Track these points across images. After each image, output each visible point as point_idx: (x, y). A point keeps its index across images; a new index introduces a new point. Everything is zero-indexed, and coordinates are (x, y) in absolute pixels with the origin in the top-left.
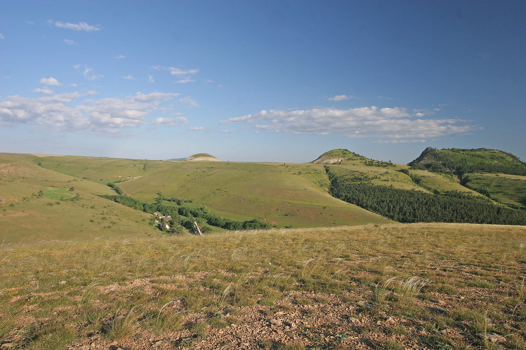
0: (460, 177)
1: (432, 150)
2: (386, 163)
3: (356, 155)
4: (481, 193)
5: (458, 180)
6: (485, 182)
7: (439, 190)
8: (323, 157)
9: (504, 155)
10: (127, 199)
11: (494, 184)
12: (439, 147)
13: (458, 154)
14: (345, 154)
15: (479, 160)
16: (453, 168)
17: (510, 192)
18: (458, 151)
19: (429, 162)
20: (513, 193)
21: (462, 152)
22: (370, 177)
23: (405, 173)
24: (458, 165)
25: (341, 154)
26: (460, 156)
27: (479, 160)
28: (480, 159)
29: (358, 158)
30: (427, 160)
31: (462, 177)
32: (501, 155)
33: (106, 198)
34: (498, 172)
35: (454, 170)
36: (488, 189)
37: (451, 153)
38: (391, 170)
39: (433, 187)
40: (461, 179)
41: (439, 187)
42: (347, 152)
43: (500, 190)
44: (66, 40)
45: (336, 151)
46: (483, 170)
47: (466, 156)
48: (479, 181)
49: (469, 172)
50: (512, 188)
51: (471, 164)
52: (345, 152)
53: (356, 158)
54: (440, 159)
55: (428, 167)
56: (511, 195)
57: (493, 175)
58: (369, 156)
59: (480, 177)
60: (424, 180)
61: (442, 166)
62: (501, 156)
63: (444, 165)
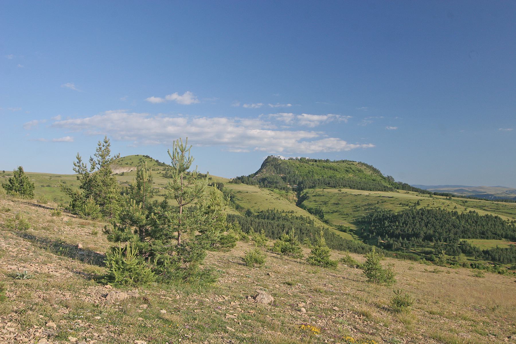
0: (298, 195)
1: (275, 159)
3: (159, 164)
5: (295, 198)
6: (323, 199)
7: (252, 210)
9: (363, 168)
11: (333, 201)
15: (330, 173)
17: (345, 211)
19: (268, 175)
20: (350, 211)
21: (312, 163)
24: (301, 179)
26: (307, 168)
27: (330, 173)
28: (332, 171)
29: (162, 168)
30: (266, 174)
32: (359, 168)
34: (345, 186)
35: (295, 186)
36: (324, 209)
39: (246, 206)
40: (299, 197)
42: (148, 159)
43: (335, 209)
44: (270, 105)
45: (130, 158)
46: (328, 185)
47: (316, 167)
48: (317, 198)
49: (310, 188)
50: (350, 206)
51: (316, 177)
54: (281, 171)
56: (347, 215)
57: (335, 191)
62: (349, 166)
63: (284, 179)
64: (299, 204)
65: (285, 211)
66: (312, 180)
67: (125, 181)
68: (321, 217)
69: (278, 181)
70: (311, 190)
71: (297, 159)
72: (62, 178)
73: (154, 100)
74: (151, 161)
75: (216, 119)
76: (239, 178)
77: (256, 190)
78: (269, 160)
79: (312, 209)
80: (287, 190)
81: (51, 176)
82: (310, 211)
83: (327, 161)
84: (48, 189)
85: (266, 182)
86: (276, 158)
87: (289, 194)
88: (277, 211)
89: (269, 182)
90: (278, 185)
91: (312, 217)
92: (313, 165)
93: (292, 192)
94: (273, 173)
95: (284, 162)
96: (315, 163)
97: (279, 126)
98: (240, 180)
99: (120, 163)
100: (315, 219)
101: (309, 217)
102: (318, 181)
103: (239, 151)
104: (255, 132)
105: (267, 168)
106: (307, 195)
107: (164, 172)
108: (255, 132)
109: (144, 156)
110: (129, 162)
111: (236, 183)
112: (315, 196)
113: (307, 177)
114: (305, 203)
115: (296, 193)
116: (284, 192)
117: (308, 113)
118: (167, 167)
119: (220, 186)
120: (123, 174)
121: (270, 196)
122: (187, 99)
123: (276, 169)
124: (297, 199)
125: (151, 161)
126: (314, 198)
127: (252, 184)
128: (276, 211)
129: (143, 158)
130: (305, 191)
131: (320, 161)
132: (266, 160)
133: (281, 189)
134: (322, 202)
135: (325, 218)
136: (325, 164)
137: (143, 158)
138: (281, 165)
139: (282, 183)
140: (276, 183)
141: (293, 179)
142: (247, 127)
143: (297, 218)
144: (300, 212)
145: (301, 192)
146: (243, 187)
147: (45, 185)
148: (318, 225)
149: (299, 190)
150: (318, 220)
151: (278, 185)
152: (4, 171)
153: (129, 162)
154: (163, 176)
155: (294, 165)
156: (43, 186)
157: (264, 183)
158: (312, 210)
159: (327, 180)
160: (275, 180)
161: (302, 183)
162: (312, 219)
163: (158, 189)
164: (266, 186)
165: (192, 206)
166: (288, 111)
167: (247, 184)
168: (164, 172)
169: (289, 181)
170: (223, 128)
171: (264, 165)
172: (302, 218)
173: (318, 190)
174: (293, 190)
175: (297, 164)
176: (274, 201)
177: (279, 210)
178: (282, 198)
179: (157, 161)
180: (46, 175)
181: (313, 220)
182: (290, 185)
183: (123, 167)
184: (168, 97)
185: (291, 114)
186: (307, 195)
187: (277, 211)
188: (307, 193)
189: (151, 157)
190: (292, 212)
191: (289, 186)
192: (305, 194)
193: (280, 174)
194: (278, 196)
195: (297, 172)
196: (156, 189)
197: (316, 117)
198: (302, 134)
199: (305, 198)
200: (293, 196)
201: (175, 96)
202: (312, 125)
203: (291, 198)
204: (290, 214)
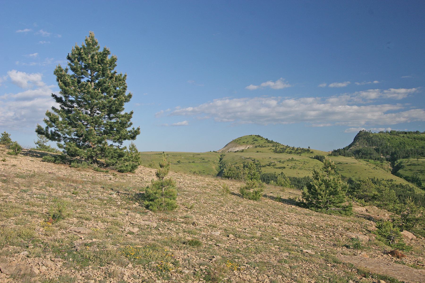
0: (392, 165)
1: (366, 133)
2: (303, 149)
3: (269, 142)
4: (409, 181)
5: (390, 167)
6: (419, 168)
7: (353, 179)
8: (229, 146)
10: (37, 156)
12: (375, 130)
13: (396, 137)
14: (256, 140)
16: (387, 153)
18: (398, 133)
19: (361, 147)
21: (402, 135)
22: (262, 164)
23: (320, 160)
24: (394, 150)
25: (251, 140)
26: (398, 139)
29: (271, 145)
30: (359, 146)
31: (394, 164)
33: (33, 156)
37: (388, 136)
38: (304, 157)
39: (348, 175)
40: (393, 167)
41: (355, 174)
42: (259, 139)
45: (246, 138)
47: (407, 139)
48: (412, 167)
49: (404, 158)
51: (408, 148)
52: (256, 139)
53: (269, 144)
54: (373, 143)
55: (358, 154)
58: (284, 142)
59: (416, 162)
60: (340, 167)
61: (375, 152)
63: (377, 150)
64: (395, 172)
65: (385, 180)
66: (404, 151)
67: (248, 157)
68: (419, 185)
69: (372, 152)
70: (405, 160)
71: (387, 132)
72: (202, 156)
73: (252, 87)
74: (262, 139)
75: (302, 100)
76: (335, 151)
77: (354, 162)
78: (361, 134)
79: (408, 177)
80: (382, 160)
81: (194, 155)
82: (406, 178)
83: (417, 132)
84: (193, 164)
85: (360, 153)
86: (367, 132)
87: (384, 164)
88: (377, 179)
89: (363, 154)
90: (372, 156)
91: (411, 185)
92: (403, 137)
93: (386, 162)
94: (366, 146)
95: (376, 136)
96: (405, 135)
97: (366, 102)
98: (336, 153)
99: (238, 142)
100: (414, 186)
101: (408, 185)
102: (411, 152)
103: (322, 125)
104: (340, 108)
105: (360, 141)
106: (402, 164)
107: (274, 148)
108: (340, 108)
109: (256, 136)
110: (246, 141)
111: (335, 155)
112: (410, 165)
113: (399, 148)
114: (400, 171)
115: (390, 163)
116: (379, 162)
117: (394, 88)
118: (275, 144)
119: (319, 158)
120: (243, 151)
121: (367, 167)
122: (279, 85)
123: (368, 142)
124: (391, 168)
125: (262, 139)
126: (409, 168)
127: (348, 155)
128: (376, 180)
129: (256, 138)
130: (399, 161)
131: (409, 133)
132: (358, 134)
133: (375, 159)
134: (418, 170)
135: (423, 185)
136: (416, 135)
137: (256, 138)
138: (373, 138)
139: (376, 155)
140: (370, 154)
141: (385, 150)
142: (333, 104)
143: (397, 186)
144: (398, 181)
145: (396, 162)
146: (341, 159)
147: (191, 161)
148: (419, 192)
149: (392, 160)
150: (417, 188)
151: (372, 156)
152: (163, 152)
153: (246, 141)
154: (274, 152)
155: (385, 138)
156: (189, 162)
157: (358, 154)
158: (409, 179)
159: (420, 150)
160: (369, 152)
161: (395, 153)
162: (411, 187)
163: (274, 162)
164: (361, 158)
165: (305, 177)
166: (374, 87)
167: (344, 156)
168: (274, 148)
169: (382, 152)
170: (311, 107)
171: (356, 139)
172: (401, 186)
173: (412, 160)
174: (387, 160)
175: (388, 136)
176: (372, 171)
177: (379, 179)
178: (378, 168)
179: (267, 139)
180: (190, 154)
181: (413, 187)
182: (383, 155)
183: (241, 145)
184: (263, 84)
185: (378, 89)
186: (402, 164)
187: (377, 179)
188: (401, 162)
189: (261, 136)
190: (392, 180)
191: (382, 157)
192: (399, 164)
193: (372, 146)
194: (375, 166)
195: (388, 144)
196: (273, 162)
197: (403, 90)
198: (387, 107)
199: (399, 167)
200: (387, 165)
201: (270, 83)
202: (400, 97)
203: (386, 167)
204: (390, 182)
